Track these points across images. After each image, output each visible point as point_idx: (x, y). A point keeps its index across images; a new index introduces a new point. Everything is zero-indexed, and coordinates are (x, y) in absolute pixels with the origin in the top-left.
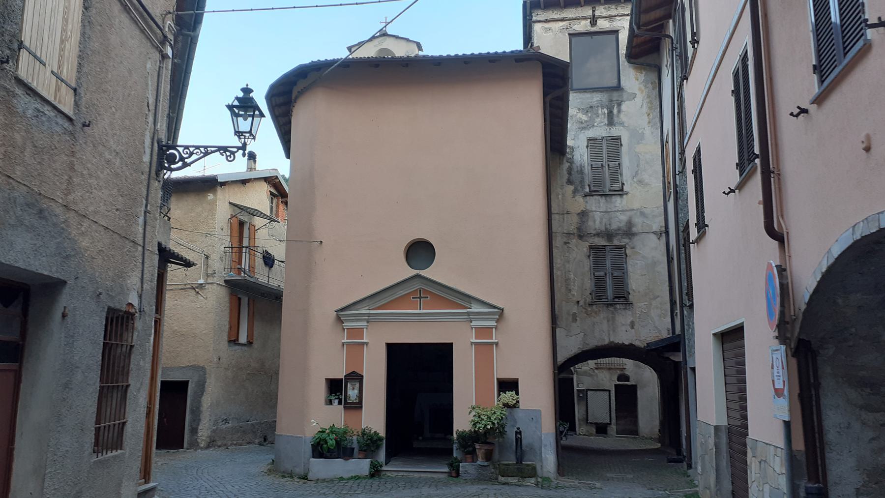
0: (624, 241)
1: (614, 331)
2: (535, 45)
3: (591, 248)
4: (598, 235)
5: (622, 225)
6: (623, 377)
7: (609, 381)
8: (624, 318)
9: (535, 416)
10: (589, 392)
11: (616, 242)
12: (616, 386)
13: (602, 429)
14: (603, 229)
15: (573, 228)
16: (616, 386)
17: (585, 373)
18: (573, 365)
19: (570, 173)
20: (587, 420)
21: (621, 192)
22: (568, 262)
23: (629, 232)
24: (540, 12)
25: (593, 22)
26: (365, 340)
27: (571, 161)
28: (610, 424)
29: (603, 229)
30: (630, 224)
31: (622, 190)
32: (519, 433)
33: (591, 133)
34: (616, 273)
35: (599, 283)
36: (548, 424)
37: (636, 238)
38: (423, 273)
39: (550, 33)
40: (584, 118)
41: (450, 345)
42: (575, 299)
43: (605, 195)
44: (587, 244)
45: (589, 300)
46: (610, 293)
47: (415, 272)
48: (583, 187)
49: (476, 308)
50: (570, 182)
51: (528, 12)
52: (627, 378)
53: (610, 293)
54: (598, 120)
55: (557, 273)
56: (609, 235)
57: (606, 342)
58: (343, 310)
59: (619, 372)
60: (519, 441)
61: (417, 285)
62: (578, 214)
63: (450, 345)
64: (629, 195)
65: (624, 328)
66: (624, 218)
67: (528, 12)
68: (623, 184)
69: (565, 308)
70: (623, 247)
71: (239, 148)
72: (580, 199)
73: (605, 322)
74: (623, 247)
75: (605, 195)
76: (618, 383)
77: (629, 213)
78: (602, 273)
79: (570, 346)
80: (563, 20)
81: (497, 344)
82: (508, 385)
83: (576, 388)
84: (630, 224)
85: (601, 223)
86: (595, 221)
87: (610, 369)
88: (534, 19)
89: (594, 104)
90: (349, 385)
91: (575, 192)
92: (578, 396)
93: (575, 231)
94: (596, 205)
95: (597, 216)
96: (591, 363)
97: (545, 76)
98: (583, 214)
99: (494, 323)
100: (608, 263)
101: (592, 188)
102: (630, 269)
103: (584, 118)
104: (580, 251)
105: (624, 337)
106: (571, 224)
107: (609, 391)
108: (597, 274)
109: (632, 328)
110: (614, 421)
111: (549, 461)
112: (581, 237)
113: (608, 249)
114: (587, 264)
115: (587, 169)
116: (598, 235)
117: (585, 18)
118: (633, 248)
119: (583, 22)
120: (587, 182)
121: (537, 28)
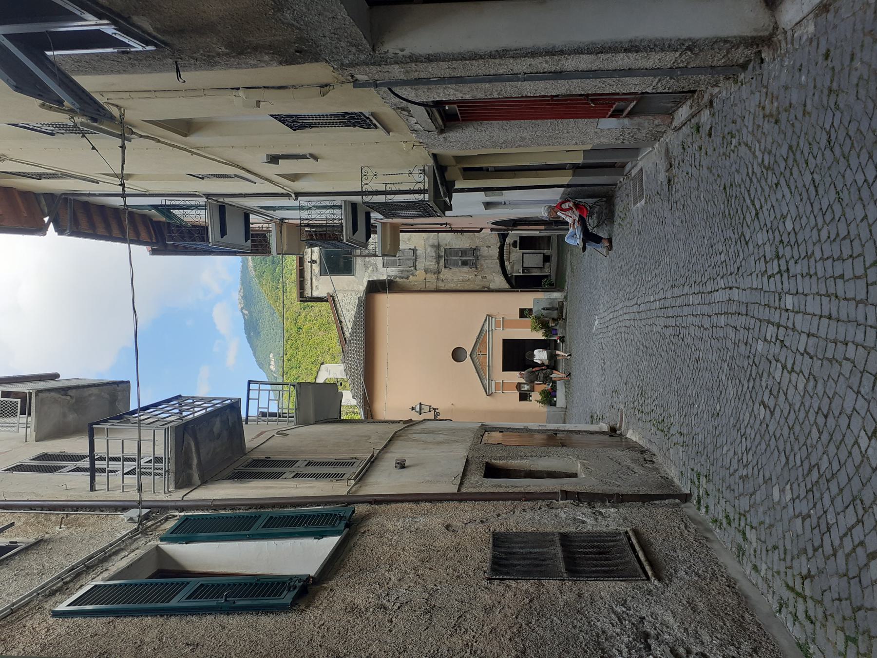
0: (442, 249)
1: (491, 257)
2: (326, 295)
3: (445, 267)
4: (438, 263)
5: (433, 250)
6: (515, 244)
7: (516, 254)
8: (484, 251)
9: (536, 301)
10: (524, 266)
11: (443, 254)
12: (520, 249)
13: (547, 259)
14: (435, 260)
15: (434, 277)
16: (520, 249)
17: (512, 268)
18: (508, 275)
19: (403, 278)
20: (541, 268)
21: (414, 251)
22: (453, 280)
23: (438, 247)
24: (306, 292)
25: (315, 262)
26: (501, 382)
27: (396, 277)
28: (543, 253)
29: (435, 260)
30: (433, 246)
31: (413, 250)
32: (544, 309)
33: (380, 265)
34: (460, 255)
35: (465, 263)
36: (541, 296)
37: (441, 243)
38: (469, 353)
39: (319, 287)
40: (371, 269)
41: (503, 340)
42: (474, 276)
43: (416, 258)
44: (443, 269)
45: (474, 269)
46: (471, 258)
47: (468, 357)
48: (411, 271)
49: (486, 327)
50: (408, 278)
51: (305, 299)
52: (515, 242)
53: (471, 258)
54: (372, 261)
55: (459, 287)
56: (439, 257)
57: (498, 261)
58: (486, 393)
59: (511, 247)
60: (547, 309)
61: (474, 356)
62: (426, 273)
63: (503, 340)
64: (416, 246)
65: (490, 251)
66: (429, 249)
67: (305, 299)
68: (410, 249)
69: (478, 283)
70: (446, 250)
71: (435, 411)
72: (417, 273)
73: (486, 261)
74: (446, 250)
75: (416, 258)
76: (518, 248)
77: (427, 247)
78: (460, 262)
79: (499, 281)
80: (312, 279)
81: (503, 318)
82: (523, 313)
83: (521, 274)
84: (433, 246)
85: (431, 261)
86: (430, 265)
87: (509, 252)
88: (310, 295)
89: (363, 263)
90: (522, 389)
91: (413, 275)
92: (526, 273)
93: (436, 275)
94: (421, 265)
95: (427, 263)
96: (506, 263)
97: (371, 292)
98: (426, 271)
99: (494, 319)
100: (454, 258)
101: (412, 265)
102: (458, 247)
103: (371, 269)
104: (446, 274)
105: (495, 252)
106: (432, 278)
107: (523, 253)
108: (460, 265)
109: (490, 247)
110: (542, 251)
111: (556, 295)
112: (439, 273)
113: (446, 258)
114: (454, 269)
115: (401, 268)
116: (438, 263)
117: (311, 266)
118: (446, 245)
119: (314, 268)
120: (408, 269)
121: (316, 294)
